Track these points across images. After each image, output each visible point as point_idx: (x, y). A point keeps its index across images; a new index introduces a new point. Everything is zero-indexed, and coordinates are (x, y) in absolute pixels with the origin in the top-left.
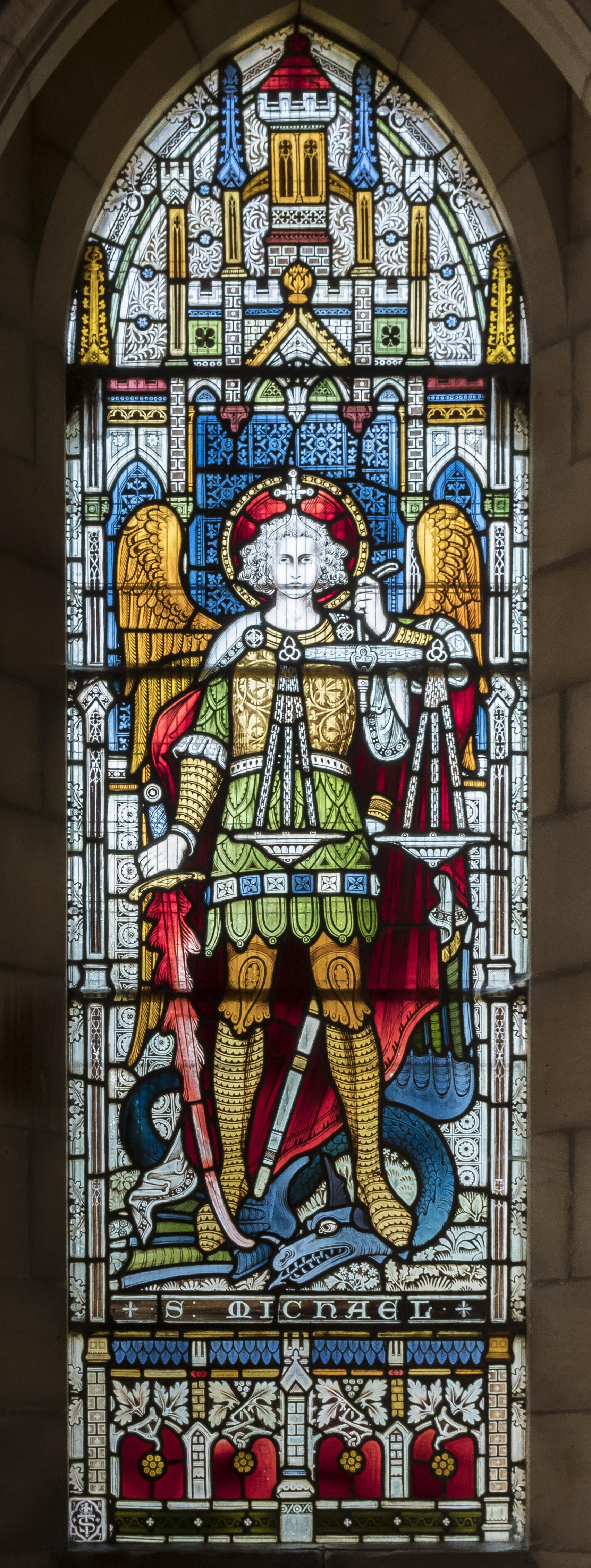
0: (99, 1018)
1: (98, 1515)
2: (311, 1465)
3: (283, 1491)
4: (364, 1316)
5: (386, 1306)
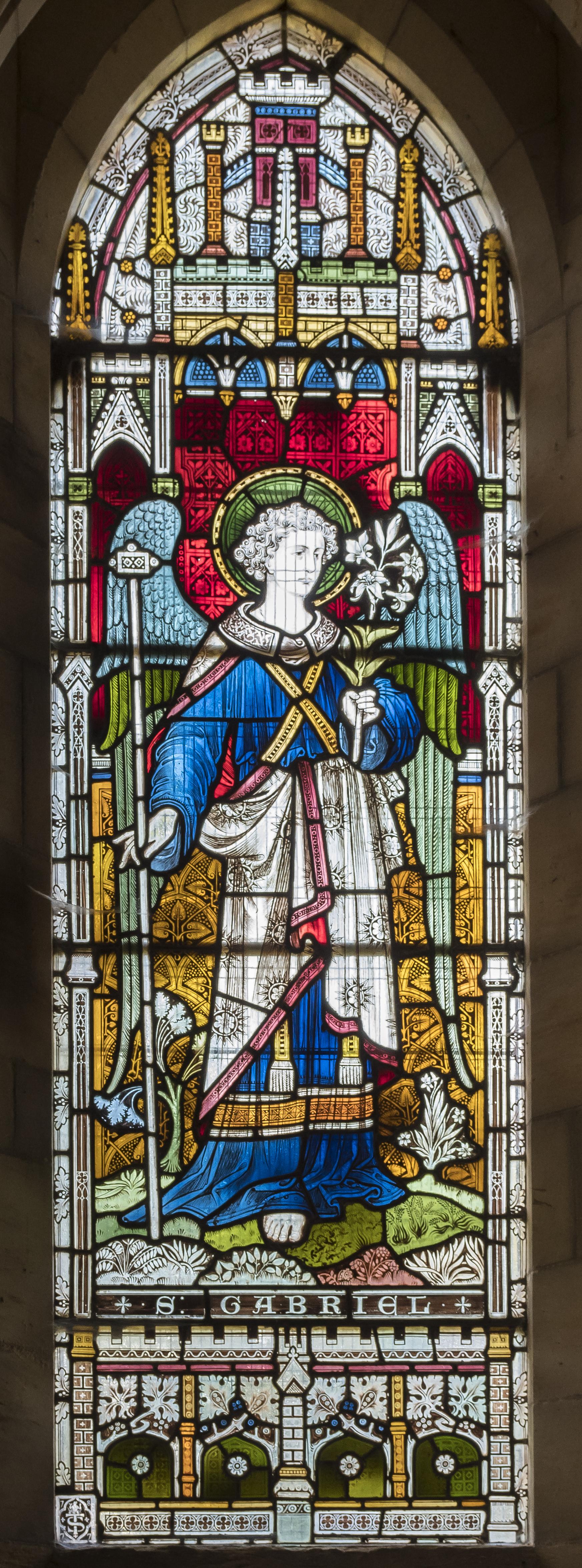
0: (500, 1007)
1: (88, 1515)
2: (311, 1465)
3: (281, 1490)
4: (270, 1311)
5: (386, 1301)
